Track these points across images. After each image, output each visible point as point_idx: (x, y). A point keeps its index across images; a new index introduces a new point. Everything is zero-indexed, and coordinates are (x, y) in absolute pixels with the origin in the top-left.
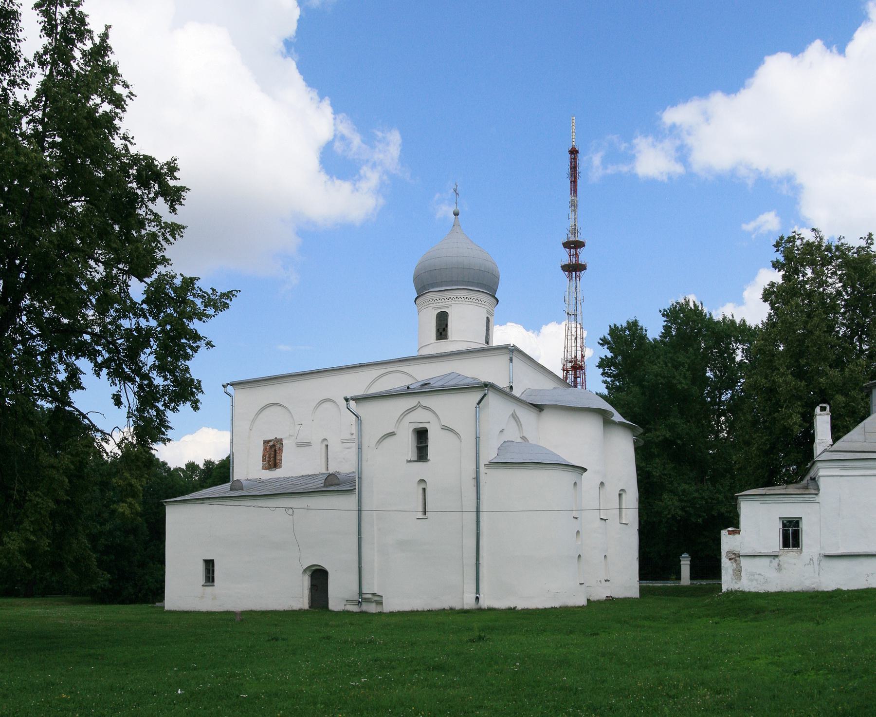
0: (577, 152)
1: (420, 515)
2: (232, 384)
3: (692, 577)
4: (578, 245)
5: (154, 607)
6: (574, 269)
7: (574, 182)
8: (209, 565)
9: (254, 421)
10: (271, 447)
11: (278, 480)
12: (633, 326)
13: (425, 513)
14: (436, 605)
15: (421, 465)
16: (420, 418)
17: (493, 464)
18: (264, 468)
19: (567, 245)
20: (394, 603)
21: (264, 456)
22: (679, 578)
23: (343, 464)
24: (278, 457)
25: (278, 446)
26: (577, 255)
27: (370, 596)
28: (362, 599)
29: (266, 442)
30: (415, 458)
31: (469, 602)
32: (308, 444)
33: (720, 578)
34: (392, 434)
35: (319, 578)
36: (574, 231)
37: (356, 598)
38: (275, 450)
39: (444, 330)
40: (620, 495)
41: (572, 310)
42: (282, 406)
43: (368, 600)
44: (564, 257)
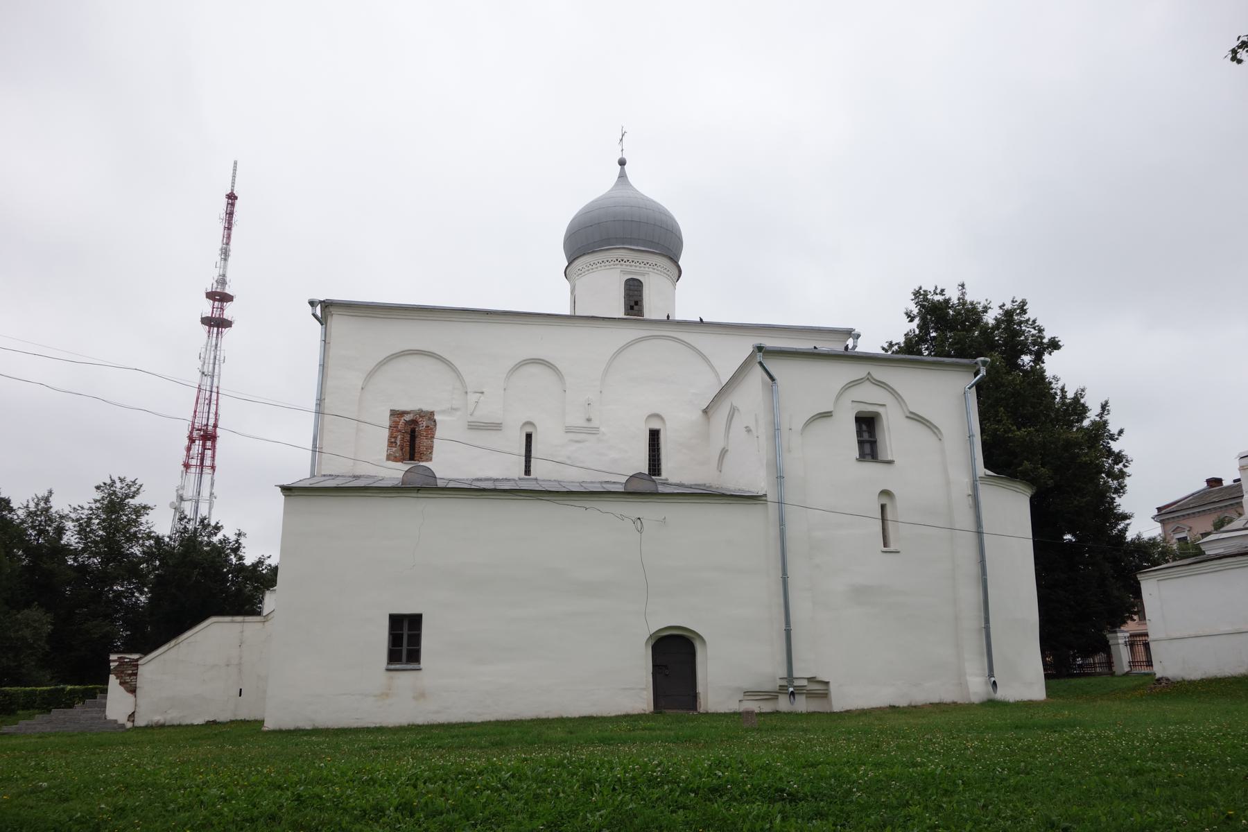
0: (236, 198)
4: (224, 298)
6: (217, 323)
7: (229, 228)
9: (371, 375)
14: (922, 696)
15: (870, 468)
16: (870, 397)
19: (211, 295)
20: (846, 697)
25: (424, 423)
26: (222, 309)
27: (805, 683)
28: (790, 688)
31: (976, 689)
32: (496, 427)
33: (107, 683)
35: (674, 655)
36: (222, 281)
39: (636, 303)
41: (208, 369)
44: (207, 308)
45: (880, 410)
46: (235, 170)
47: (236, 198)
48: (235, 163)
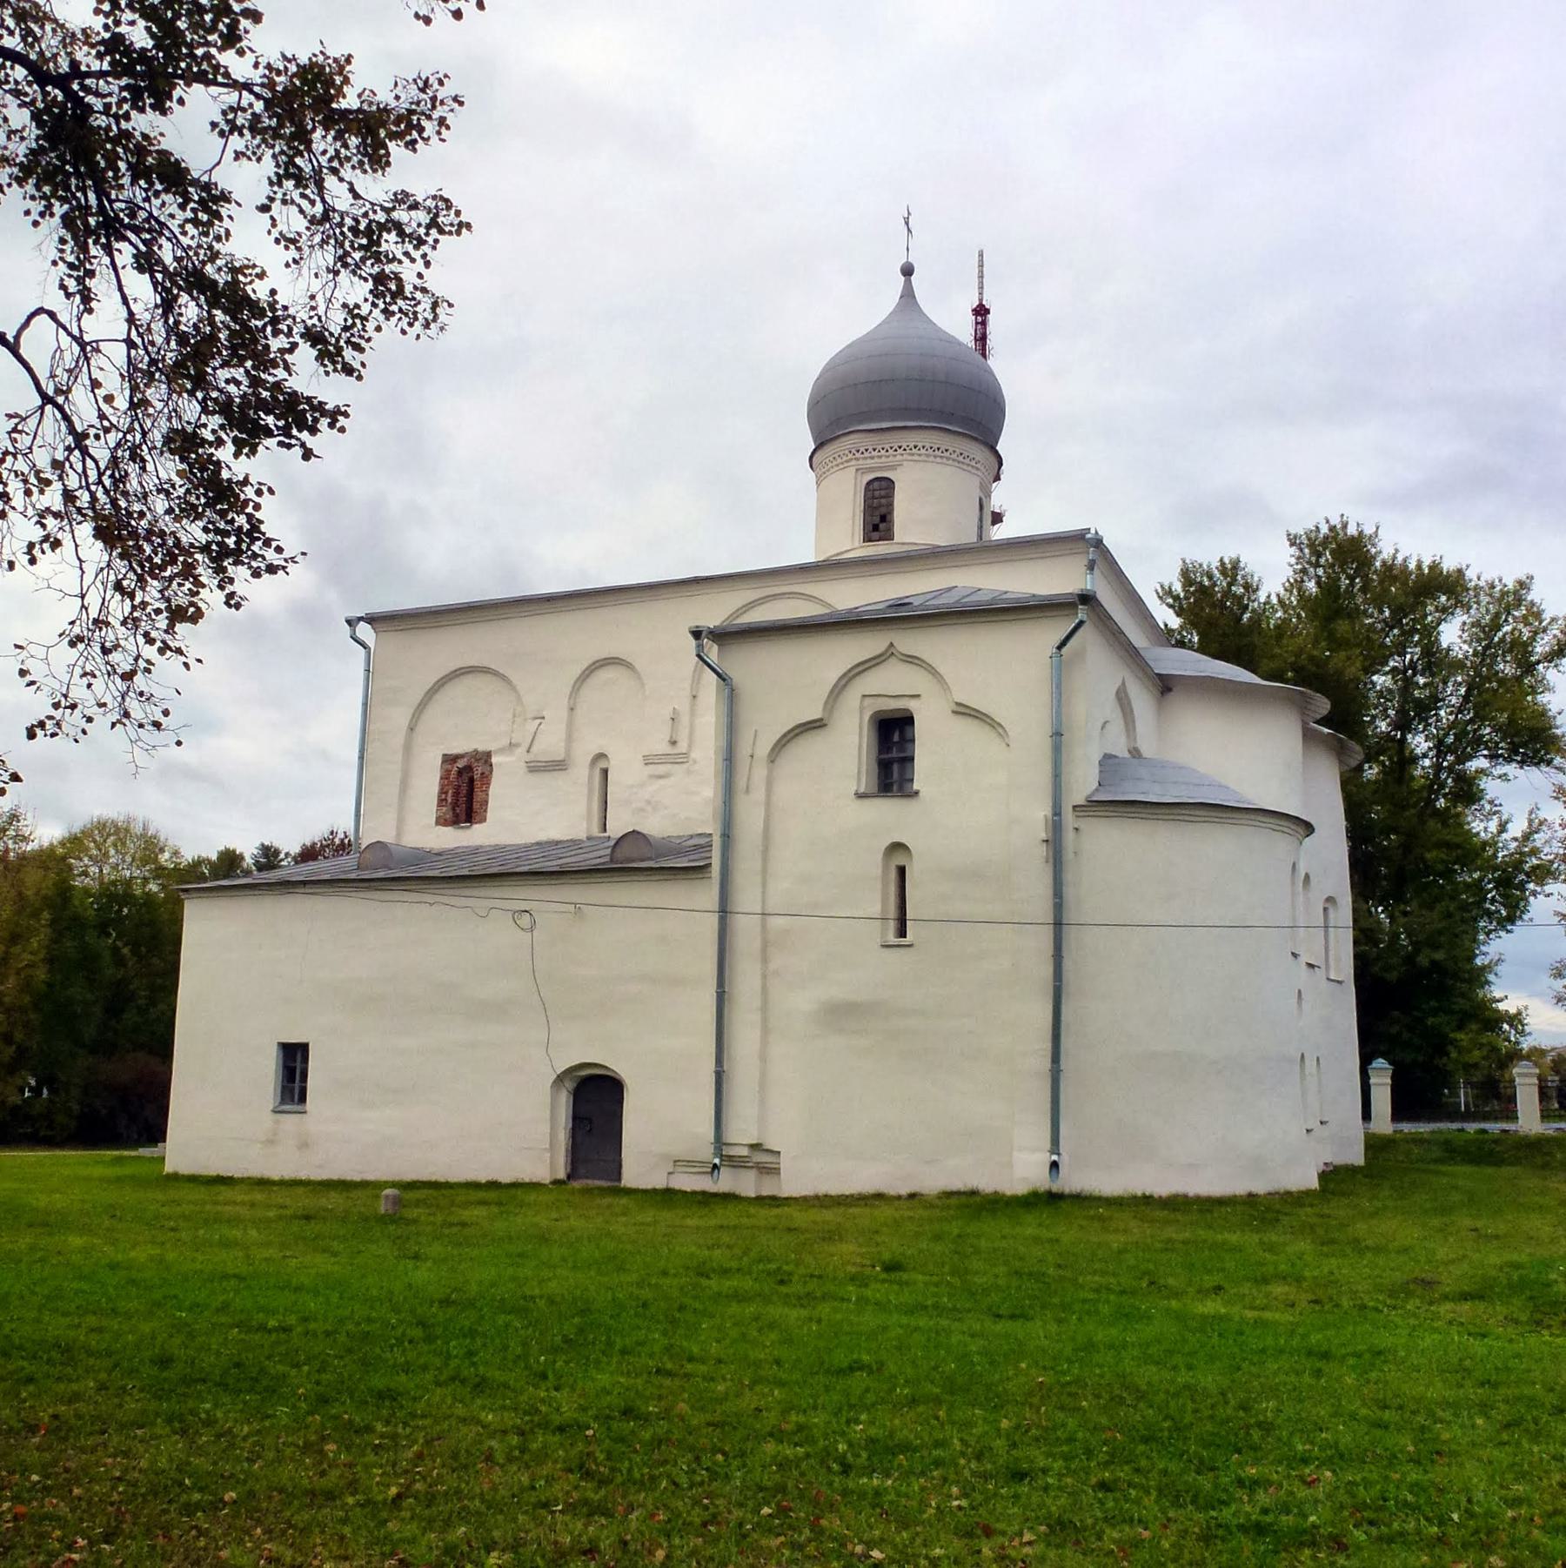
1: (892, 938)
2: (371, 620)
3: (1398, 1114)
5: (119, 1161)
8: (294, 1059)
10: (460, 772)
11: (475, 851)
12: (1231, 570)
13: (902, 933)
15: (887, 809)
16: (891, 685)
17: (1097, 807)
18: (441, 821)
20: (801, 1176)
21: (443, 791)
22: (1512, 1116)
23: (675, 806)
24: (478, 796)
25: (478, 770)
27: (744, 1152)
28: (724, 1157)
29: (449, 759)
30: (875, 789)
31: (1023, 1170)
32: (557, 766)
34: (816, 725)
35: (595, 1100)
37: (707, 1154)
38: (472, 780)
39: (883, 518)
40: (1325, 909)
42: (495, 673)
43: (735, 1163)
45: (912, 705)
46: (981, 266)
47: (988, 311)
48: (981, 255)
